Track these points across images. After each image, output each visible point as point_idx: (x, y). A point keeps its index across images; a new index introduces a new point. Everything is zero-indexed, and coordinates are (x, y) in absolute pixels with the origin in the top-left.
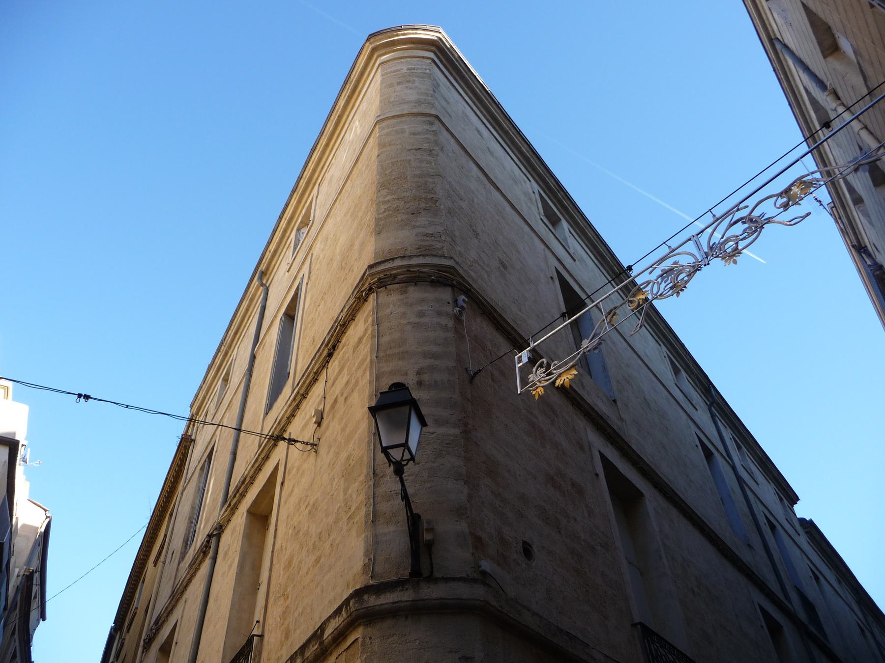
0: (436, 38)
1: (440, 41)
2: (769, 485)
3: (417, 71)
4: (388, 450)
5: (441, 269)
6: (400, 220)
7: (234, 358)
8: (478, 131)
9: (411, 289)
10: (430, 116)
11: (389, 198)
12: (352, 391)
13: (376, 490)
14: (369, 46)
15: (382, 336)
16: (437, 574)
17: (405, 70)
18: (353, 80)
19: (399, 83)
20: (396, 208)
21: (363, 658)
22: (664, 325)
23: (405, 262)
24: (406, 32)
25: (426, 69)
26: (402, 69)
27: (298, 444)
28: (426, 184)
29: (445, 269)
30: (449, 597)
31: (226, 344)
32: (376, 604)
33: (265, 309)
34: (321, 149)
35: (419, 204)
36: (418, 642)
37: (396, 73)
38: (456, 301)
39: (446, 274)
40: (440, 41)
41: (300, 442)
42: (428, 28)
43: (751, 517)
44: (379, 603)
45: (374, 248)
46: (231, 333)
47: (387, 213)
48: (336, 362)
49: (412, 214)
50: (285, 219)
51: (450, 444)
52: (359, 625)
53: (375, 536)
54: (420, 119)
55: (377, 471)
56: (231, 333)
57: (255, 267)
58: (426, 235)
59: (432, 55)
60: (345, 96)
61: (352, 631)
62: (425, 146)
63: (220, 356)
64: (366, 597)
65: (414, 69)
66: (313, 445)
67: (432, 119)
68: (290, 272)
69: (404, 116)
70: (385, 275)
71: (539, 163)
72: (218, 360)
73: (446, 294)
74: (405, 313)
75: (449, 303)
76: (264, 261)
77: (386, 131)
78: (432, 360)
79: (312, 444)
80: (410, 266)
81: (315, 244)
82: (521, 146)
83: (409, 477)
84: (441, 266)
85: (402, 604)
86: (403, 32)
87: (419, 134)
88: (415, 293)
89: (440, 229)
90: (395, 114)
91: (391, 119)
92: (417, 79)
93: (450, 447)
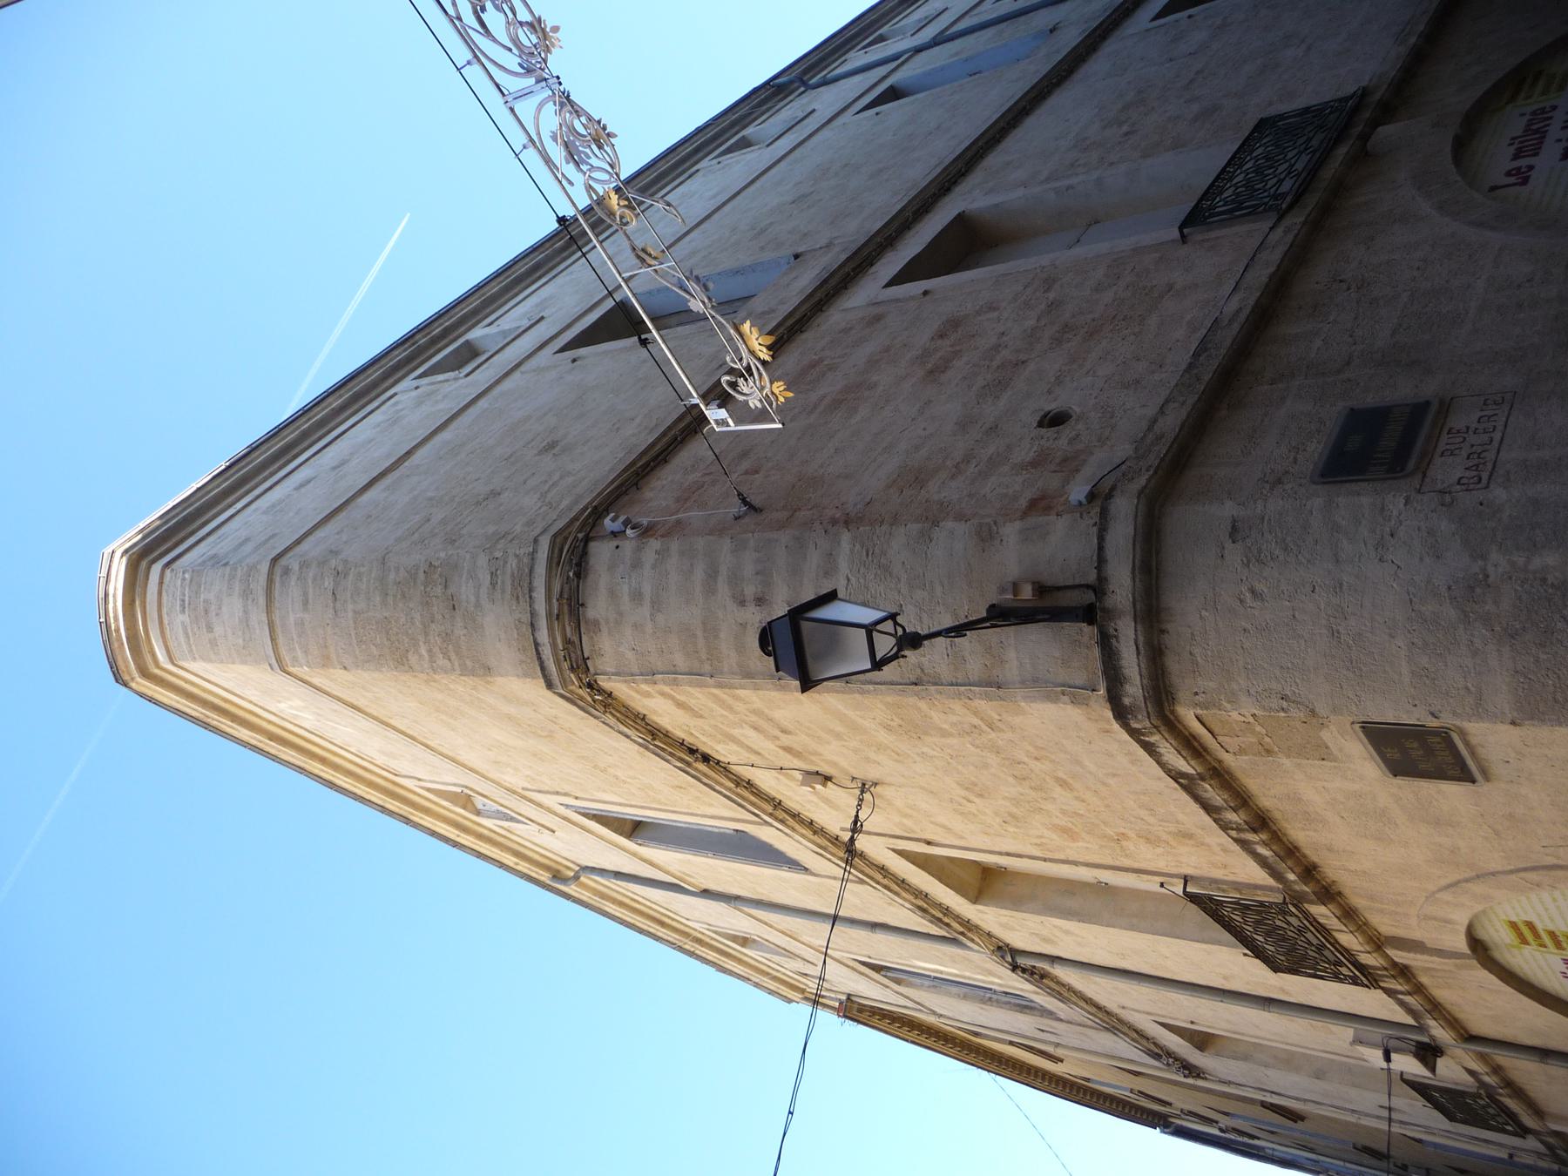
0: (124, 559)
1: (130, 553)
3: (187, 595)
6: (465, 631)
8: (302, 486)
10: (272, 574)
14: (137, 683)
16: (1092, 577)
17: (185, 618)
18: (202, 713)
19: (210, 629)
20: (442, 638)
21: (1228, 706)
22: (664, 161)
23: (542, 623)
25: (184, 579)
26: (183, 623)
27: (862, 816)
28: (399, 583)
29: (556, 551)
30: (1131, 557)
37: (191, 635)
41: (857, 812)
44: (1138, 678)
46: (661, 932)
49: (454, 609)
52: (1173, 712)
53: (1024, 683)
54: (277, 593)
55: (913, 679)
56: (661, 932)
58: (493, 584)
59: (156, 569)
62: (328, 583)
64: (1127, 701)
65: (183, 601)
67: (278, 571)
69: (273, 622)
74: (635, 626)
77: (299, 654)
78: (720, 579)
79: (862, 792)
80: (549, 614)
84: (550, 559)
85: (1141, 639)
86: (112, 621)
87: (305, 594)
88: (597, 607)
89: (482, 560)
90: (269, 637)
91: (276, 645)
92: (202, 596)
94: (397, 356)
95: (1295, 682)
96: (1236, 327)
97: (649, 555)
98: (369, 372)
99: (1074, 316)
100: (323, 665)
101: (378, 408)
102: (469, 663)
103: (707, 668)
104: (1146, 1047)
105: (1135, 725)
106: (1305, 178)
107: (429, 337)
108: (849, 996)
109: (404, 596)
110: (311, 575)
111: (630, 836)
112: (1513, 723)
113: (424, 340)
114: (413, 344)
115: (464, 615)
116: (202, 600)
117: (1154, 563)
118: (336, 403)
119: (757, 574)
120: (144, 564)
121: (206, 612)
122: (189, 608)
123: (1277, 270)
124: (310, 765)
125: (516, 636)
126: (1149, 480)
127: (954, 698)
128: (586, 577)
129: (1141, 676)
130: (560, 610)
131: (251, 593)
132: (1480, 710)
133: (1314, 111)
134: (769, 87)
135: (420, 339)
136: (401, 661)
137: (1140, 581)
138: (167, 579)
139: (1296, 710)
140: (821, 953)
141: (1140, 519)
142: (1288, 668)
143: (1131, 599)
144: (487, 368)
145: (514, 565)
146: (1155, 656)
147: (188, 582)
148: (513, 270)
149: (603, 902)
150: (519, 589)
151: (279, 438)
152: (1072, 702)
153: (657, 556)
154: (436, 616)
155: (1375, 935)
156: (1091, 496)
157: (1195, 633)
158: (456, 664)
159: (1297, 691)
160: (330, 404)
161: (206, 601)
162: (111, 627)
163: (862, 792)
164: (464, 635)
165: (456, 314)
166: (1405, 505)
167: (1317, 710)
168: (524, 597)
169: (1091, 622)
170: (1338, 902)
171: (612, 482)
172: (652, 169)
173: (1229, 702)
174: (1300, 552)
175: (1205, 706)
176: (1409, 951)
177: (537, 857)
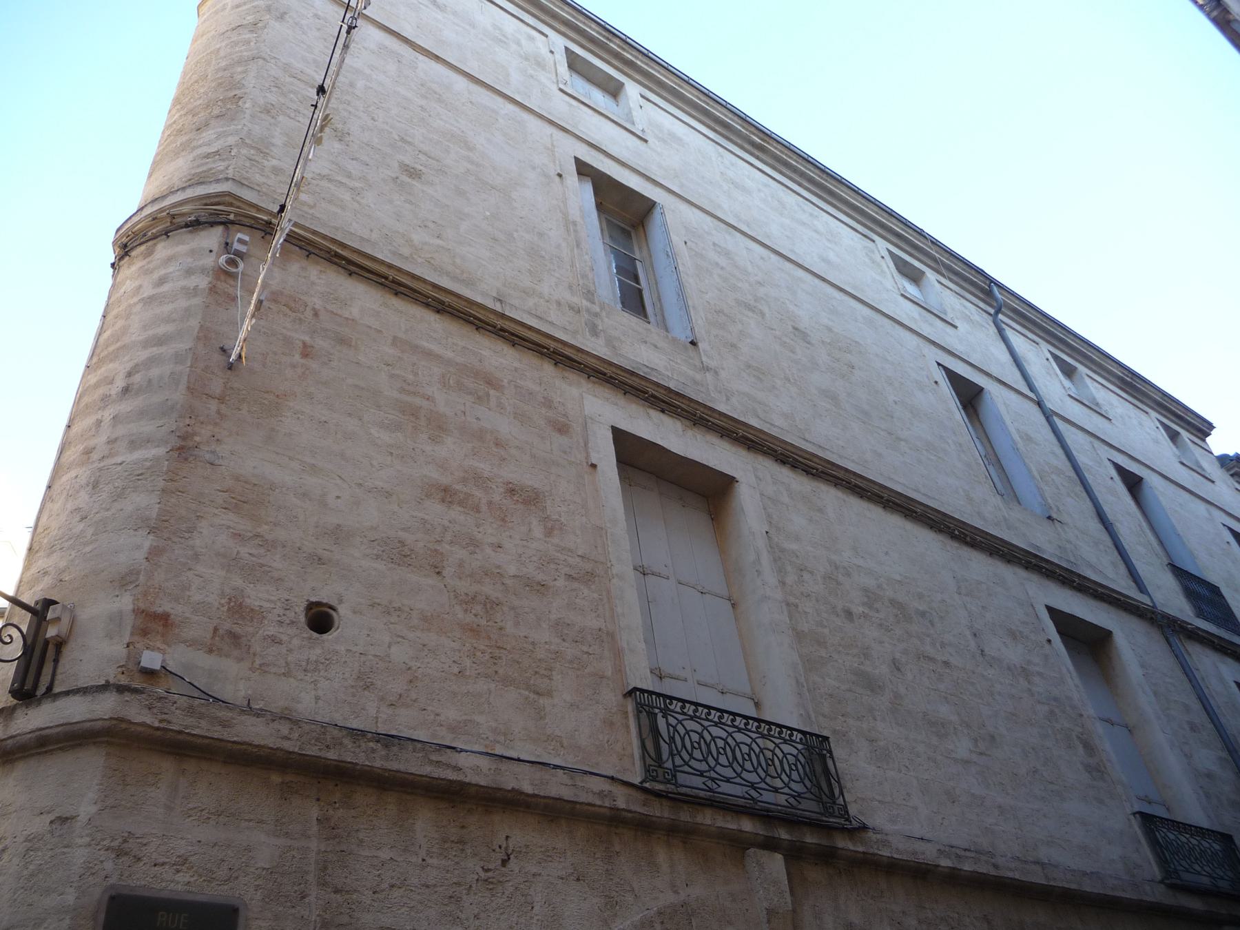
2: (1143, 416)
5: (208, 202)
22: (876, 209)
29: (217, 200)
30: (51, 725)
43: (1073, 474)
51: (141, 474)
71: (581, 18)
82: (633, 59)
84: (208, 196)
93: (141, 480)
94: (590, 28)
96: (427, 770)
99: (513, 608)
101: (528, 25)
106: (701, 798)
107: (619, 50)
113: (615, 47)
114: (608, 39)
117: (51, 748)
123: (528, 795)
126: (143, 724)
128: (190, 232)
133: (830, 785)
134: (988, 282)
135: (615, 44)
137: (31, 738)
141: (88, 725)
144: (571, 105)
148: (716, 106)
154: (196, 118)
156: (149, 673)
165: (652, 68)
171: (315, 233)
172: (863, 201)
174: (26, 890)
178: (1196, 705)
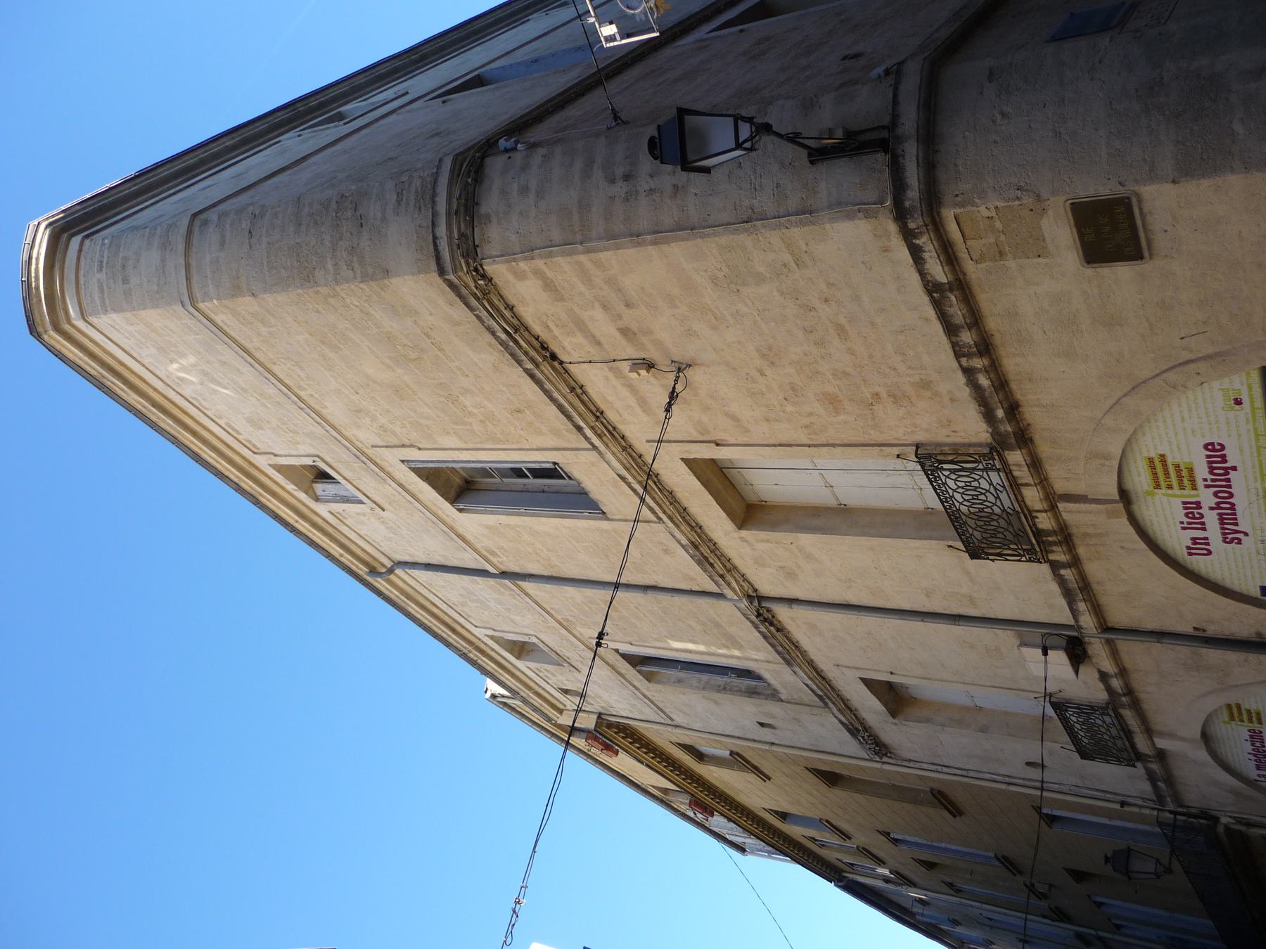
0: (48, 230)
1: (54, 226)
3: (105, 256)
4: (740, 142)
6: (370, 243)
7: (491, 633)
8: (203, 189)
9: (483, 209)
10: (192, 226)
11: (330, 266)
12: (619, 290)
13: (769, 217)
14: (49, 336)
15: (551, 241)
17: (102, 276)
18: (99, 373)
19: (126, 281)
20: (348, 252)
23: (442, 221)
24: (33, 275)
25: (103, 244)
26: (99, 281)
27: (679, 388)
28: (313, 214)
29: (458, 166)
31: (466, 648)
32: (917, 189)
33: (429, 564)
34: (199, 444)
35: (347, 219)
36: (967, 133)
37: (105, 287)
38: (506, 150)
39: (464, 166)
40: (54, 226)
41: (675, 385)
42: (29, 240)
45: (410, 277)
46: (453, 638)
47: (356, 265)
48: (567, 342)
49: (362, 226)
50: (297, 522)
52: (939, 214)
53: (830, 207)
54: (195, 242)
55: (745, 218)
56: (453, 638)
57: (360, 585)
58: (399, 202)
59: (75, 242)
60: (122, 390)
61: (944, 230)
62: (245, 224)
63: (484, 662)
64: (907, 204)
65: (102, 262)
66: (679, 370)
67: (197, 223)
68: (385, 505)
69: (189, 264)
70: (459, 248)
72: (488, 664)
73: (495, 164)
74: (521, 214)
75: (510, 158)
76: (354, 568)
77: (211, 288)
78: (595, 167)
79: (678, 373)
80: (448, 214)
81: (357, 443)
83: (757, 172)
84: (452, 171)
86: (33, 280)
87: (223, 236)
88: (491, 202)
89: (390, 185)
90: (184, 276)
91: (190, 283)
92: (121, 255)
95: (1028, 174)
97: (537, 158)
98: (257, 124)
100: (233, 295)
102: (370, 270)
103: (579, 237)
104: (848, 720)
105: (912, 225)
108: (600, 715)
109: (316, 223)
110: (229, 221)
111: (453, 502)
112: (1174, 182)
115: (370, 229)
116: (120, 257)
118: (229, 142)
119: (626, 158)
120: (65, 236)
121: (124, 267)
122: (107, 267)
124: (183, 435)
125: (415, 238)
127: (775, 230)
129: (919, 181)
130: (458, 207)
131: (170, 245)
132: (1152, 176)
135: (300, 107)
136: (307, 278)
138: (85, 248)
139: (1027, 197)
140: (591, 649)
142: (1023, 165)
143: (915, 127)
145: (418, 185)
146: (930, 167)
147: (107, 246)
149: (408, 602)
150: (422, 201)
151: (181, 161)
152: (865, 217)
153: (543, 159)
155: (1051, 494)
157: (959, 149)
158: (358, 272)
159: (1028, 182)
160: (224, 143)
161: (126, 259)
162: (31, 285)
163: (678, 373)
164: (369, 246)
166: (1110, 41)
167: (1041, 194)
168: (425, 206)
169: (886, 151)
170: (1029, 449)
173: (979, 198)
175: (962, 205)
176: (1075, 503)
177: (359, 552)
178: (664, 709)
